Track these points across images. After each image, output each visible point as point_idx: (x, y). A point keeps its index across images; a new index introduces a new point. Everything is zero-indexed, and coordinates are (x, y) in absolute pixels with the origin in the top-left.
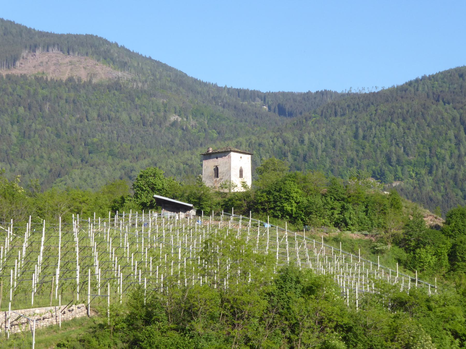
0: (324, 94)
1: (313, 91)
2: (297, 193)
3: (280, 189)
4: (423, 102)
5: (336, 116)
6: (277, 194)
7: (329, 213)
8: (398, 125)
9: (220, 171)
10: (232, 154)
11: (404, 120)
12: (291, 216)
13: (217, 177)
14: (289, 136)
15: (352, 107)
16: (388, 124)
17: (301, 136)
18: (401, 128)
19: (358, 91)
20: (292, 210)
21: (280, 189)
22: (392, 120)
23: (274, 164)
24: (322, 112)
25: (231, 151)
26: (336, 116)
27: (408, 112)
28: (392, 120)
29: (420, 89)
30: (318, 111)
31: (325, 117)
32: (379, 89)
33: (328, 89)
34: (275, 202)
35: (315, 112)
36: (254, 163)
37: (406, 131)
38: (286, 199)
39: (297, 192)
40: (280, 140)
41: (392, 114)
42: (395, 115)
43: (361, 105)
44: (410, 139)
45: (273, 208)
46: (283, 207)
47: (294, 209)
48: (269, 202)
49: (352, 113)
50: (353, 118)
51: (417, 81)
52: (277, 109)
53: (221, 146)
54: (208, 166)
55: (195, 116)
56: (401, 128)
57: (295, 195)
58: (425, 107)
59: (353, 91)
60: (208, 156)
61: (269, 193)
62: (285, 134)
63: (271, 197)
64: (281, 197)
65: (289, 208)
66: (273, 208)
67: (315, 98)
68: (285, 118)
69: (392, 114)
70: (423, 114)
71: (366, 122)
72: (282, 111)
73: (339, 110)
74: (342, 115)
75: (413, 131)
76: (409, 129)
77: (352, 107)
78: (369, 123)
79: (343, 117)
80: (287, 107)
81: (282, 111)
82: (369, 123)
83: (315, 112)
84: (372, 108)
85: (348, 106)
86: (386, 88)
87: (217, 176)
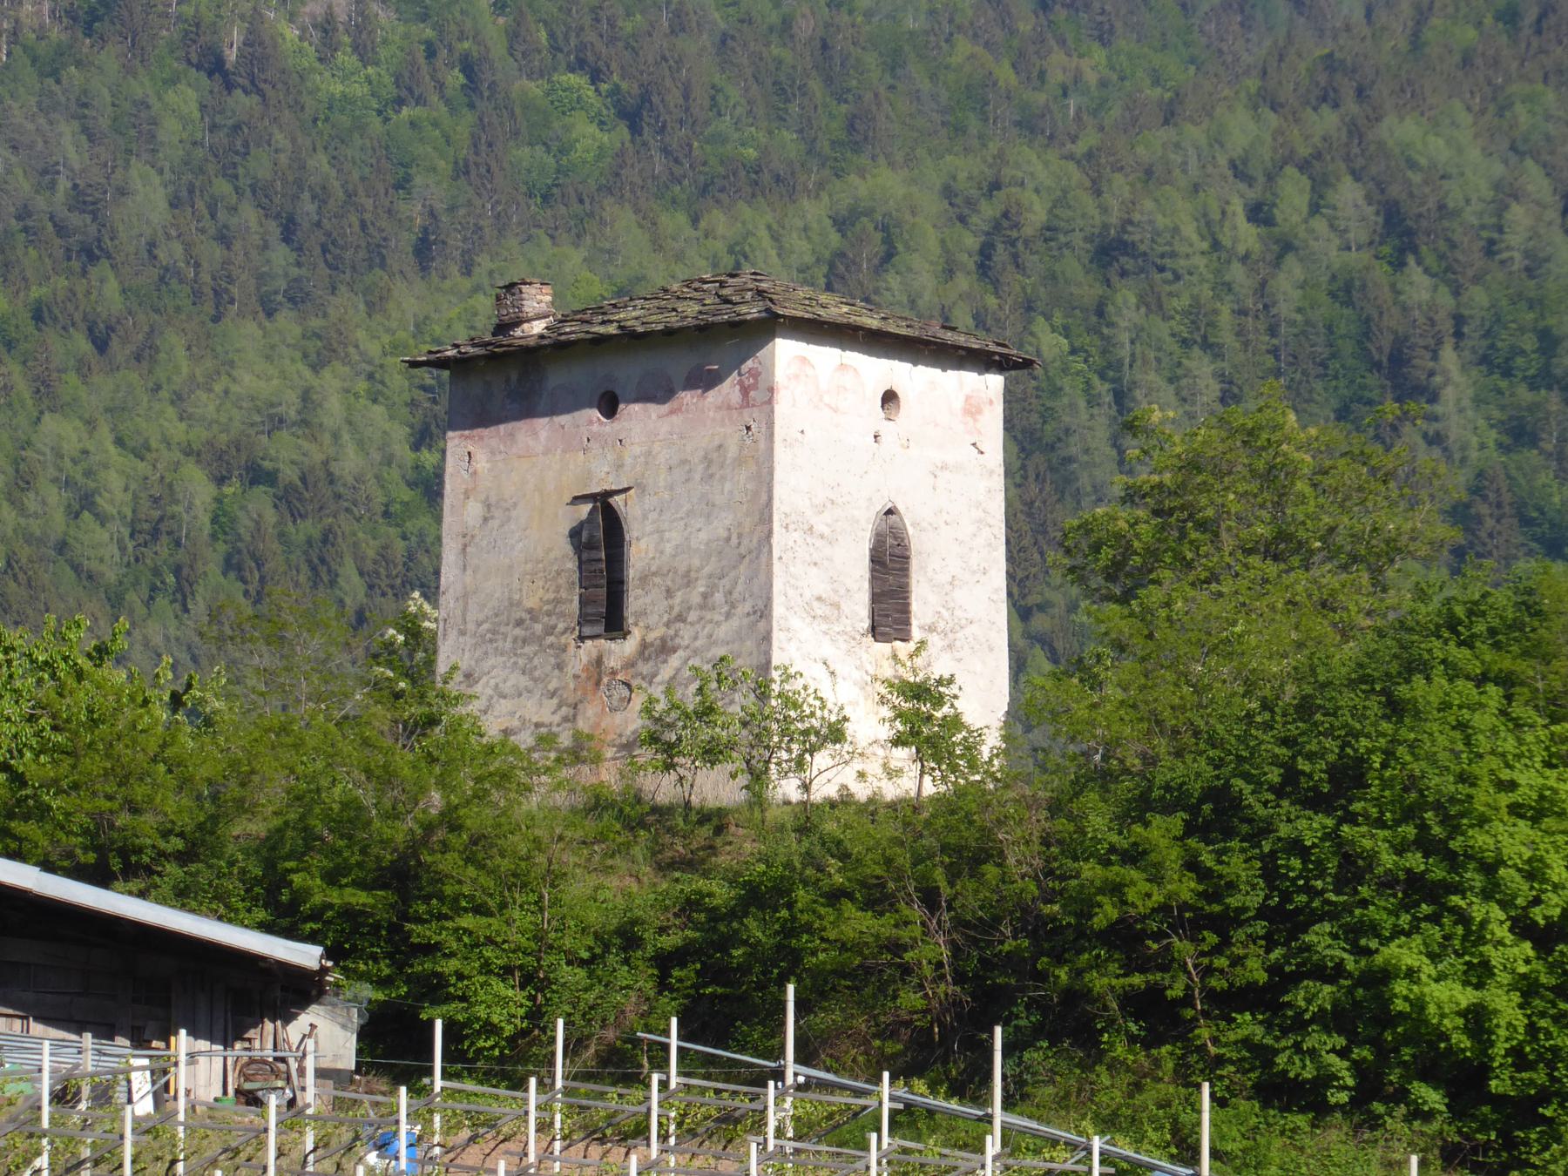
6: (1311, 827)
9: (640, 553)
10: (787, 356)
13: (613, 623)
20: (1477, 1020)
25: (772, 325)
34: (1286, 922)
36: (1033, 450)
38: (1415, 888)
40: (1348, 194)
45: (1264, 999)
47: (1507, 1009)
48: (1212, 919)
53: (656, 263)
60: (502, 379)
61: (1215, 815)
62: (1401, 130)
63: (1238, 865)
64: (1353, 868)
65: (1446, 997)
66: (1264, 999)
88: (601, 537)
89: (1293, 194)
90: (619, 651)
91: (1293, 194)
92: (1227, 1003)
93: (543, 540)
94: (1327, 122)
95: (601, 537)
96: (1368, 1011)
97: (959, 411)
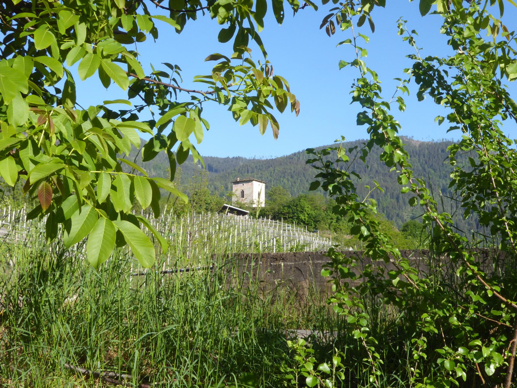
0: (238, 159)
1: (231, 157)
2: (308, 208)
3: (297, 205)
4: (304, 166)
5: (248, 173)
6: (295, 208)
7: (329, 221)
8: (288, 180)
9: (245, 193)
10: (254, 182)
11: (292, 177)
12: (304, 223)
13: (243, 197)
14: (218, 184)
15: (258, 168)
16: (282, 179)
17: (226, 185)
18: (290, 182)
19: (259, 158)
20: (305, 219)
21: (297, 205)
22: (284, 177)
23: (280, 190)
24: (239, 169)
25: (253, 180)
26: (248, 173)
27: (294, 172)
28: (284, 177)
29: (301, 158)
30: (237, 169)
31: (241, 173)
32: (265, 159)
33: (240, 156)
34: (293, 213)
35: (235, 170)
36: (266, 187)
37: (293, 184)
38: (301, 212)
39: (308, 207)
40: (213, 186)
41: (284, 173)
42: (286, 174)
43: (264, 166)
44: (295, 189)
45: (292, 218)
46: (299, 217)
47: (307, 219)
48: (289, 213)
49: (258, 172)
50: (260, 174)
51: (299, 153)
52: (207, 167)
53: (247, 177)
54: (237, 189)
55: (155, 169)
56: (290, 182)
57: (307, 209)
58: (304, 169)
59: (256, 158)
60: (237, 183)
61: (289, 207)
62: (215, 183)
63: (290, 210)
64: (297, 210)
65: (303, 218)
66: (292, 218)
67: (232, 161)
68: (212, 173)
69: (284, 173)
70: (304, 174)
71: (267, 178)
72: (210, 168)
73: (250, 169)
74: (251, 173)
75: (297, 184)
76: (295, 183)
77: (258, 168)
78: (270, 178)
79: (253, 174)
80: (214, 166)
81: (210, 168)
82: (270, 178)
83: (235, 170)
84: (271, 169)
85: (256, 167)
86: (279, 156)
87: (243, 196)
88: (243, 192)
89: (209, 186)
90: (243, 199)
91: (209, 186)
92: (289, 218)
93: (239, 193)
94: (211, 182)
95: (243, 192)
96: (298, 218)
97: (263, 185)
